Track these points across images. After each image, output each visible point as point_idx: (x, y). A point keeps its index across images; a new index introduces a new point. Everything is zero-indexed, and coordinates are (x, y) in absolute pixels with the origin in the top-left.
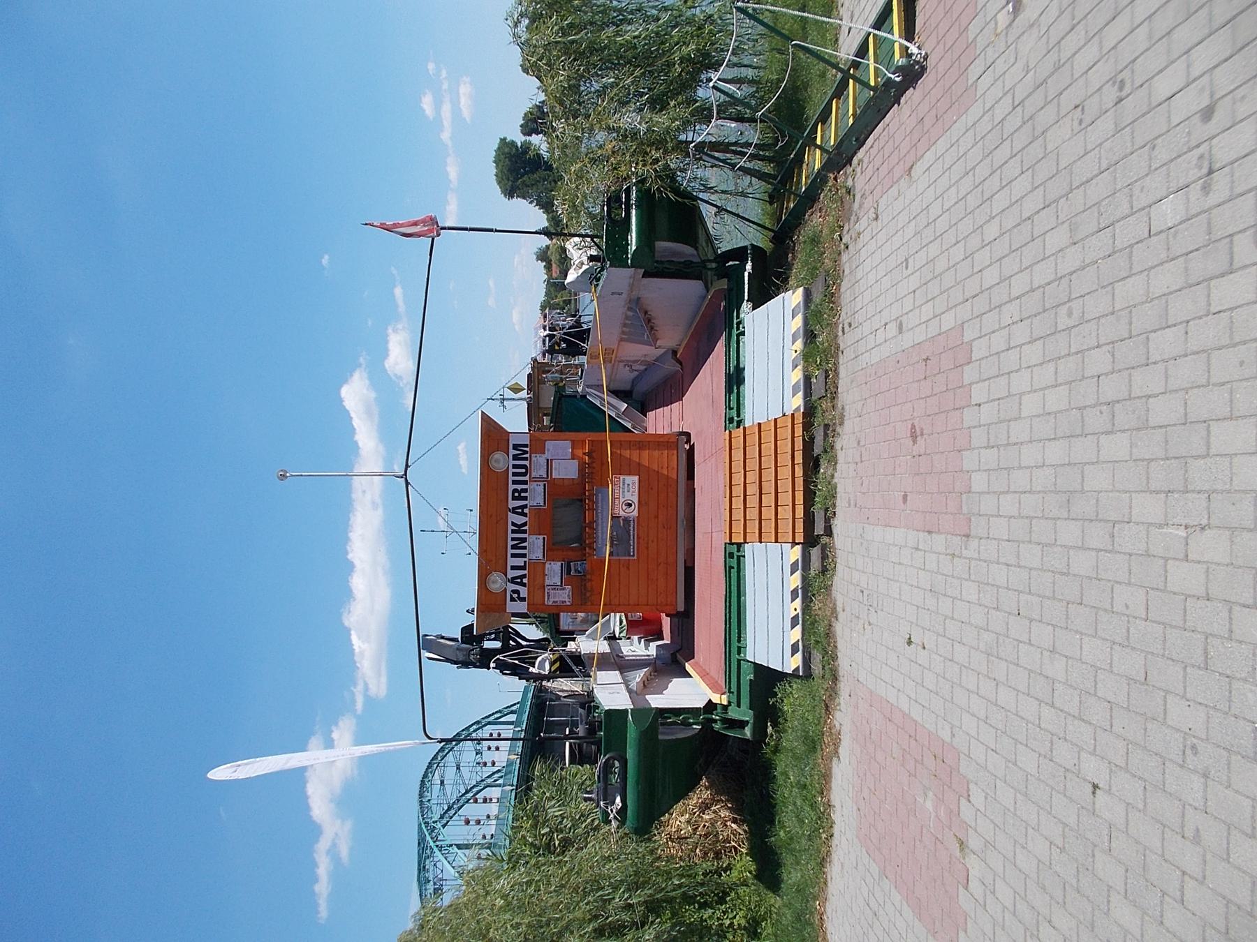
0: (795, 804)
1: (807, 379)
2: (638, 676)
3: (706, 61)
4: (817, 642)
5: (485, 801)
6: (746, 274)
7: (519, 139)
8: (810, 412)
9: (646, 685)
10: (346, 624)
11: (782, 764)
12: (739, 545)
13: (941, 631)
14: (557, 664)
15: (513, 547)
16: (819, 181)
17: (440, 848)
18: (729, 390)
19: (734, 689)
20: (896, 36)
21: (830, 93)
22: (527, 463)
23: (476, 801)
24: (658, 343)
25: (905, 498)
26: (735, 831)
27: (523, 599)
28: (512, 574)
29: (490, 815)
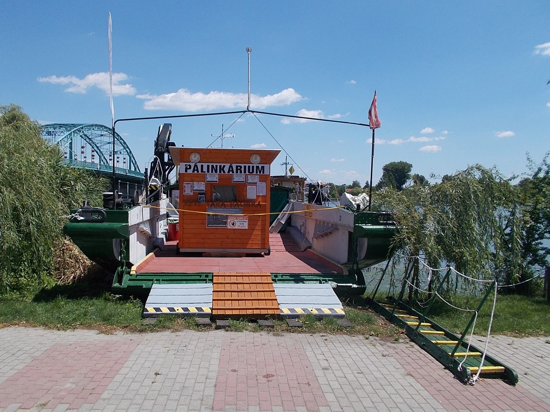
0: (77, 310)
1: (298, 316)
2: (147, 229)
3: (461, 266)
4: (160, 322)
5: (93, 156)
6: (351, 285)
7: (412, 173)
8: (281, 318)
9: (141, 233)
10: (180, 90)
11: (99, 303)
12: (212, 280)
13: (162, 393)
14: (154, 189)
15: (213, 166)
16: (401, 324)
17: (70, 134)
18: (292, 275)
19: (139, 277)
20: (482, 368)
21: (447, 330)
22: (255, 173)
23: (93, 151)
24: (315, 239)
25: (234, 371)
26: (70, 277)
27: (186, 171)
28: (199, 165)
29: (84, 156)
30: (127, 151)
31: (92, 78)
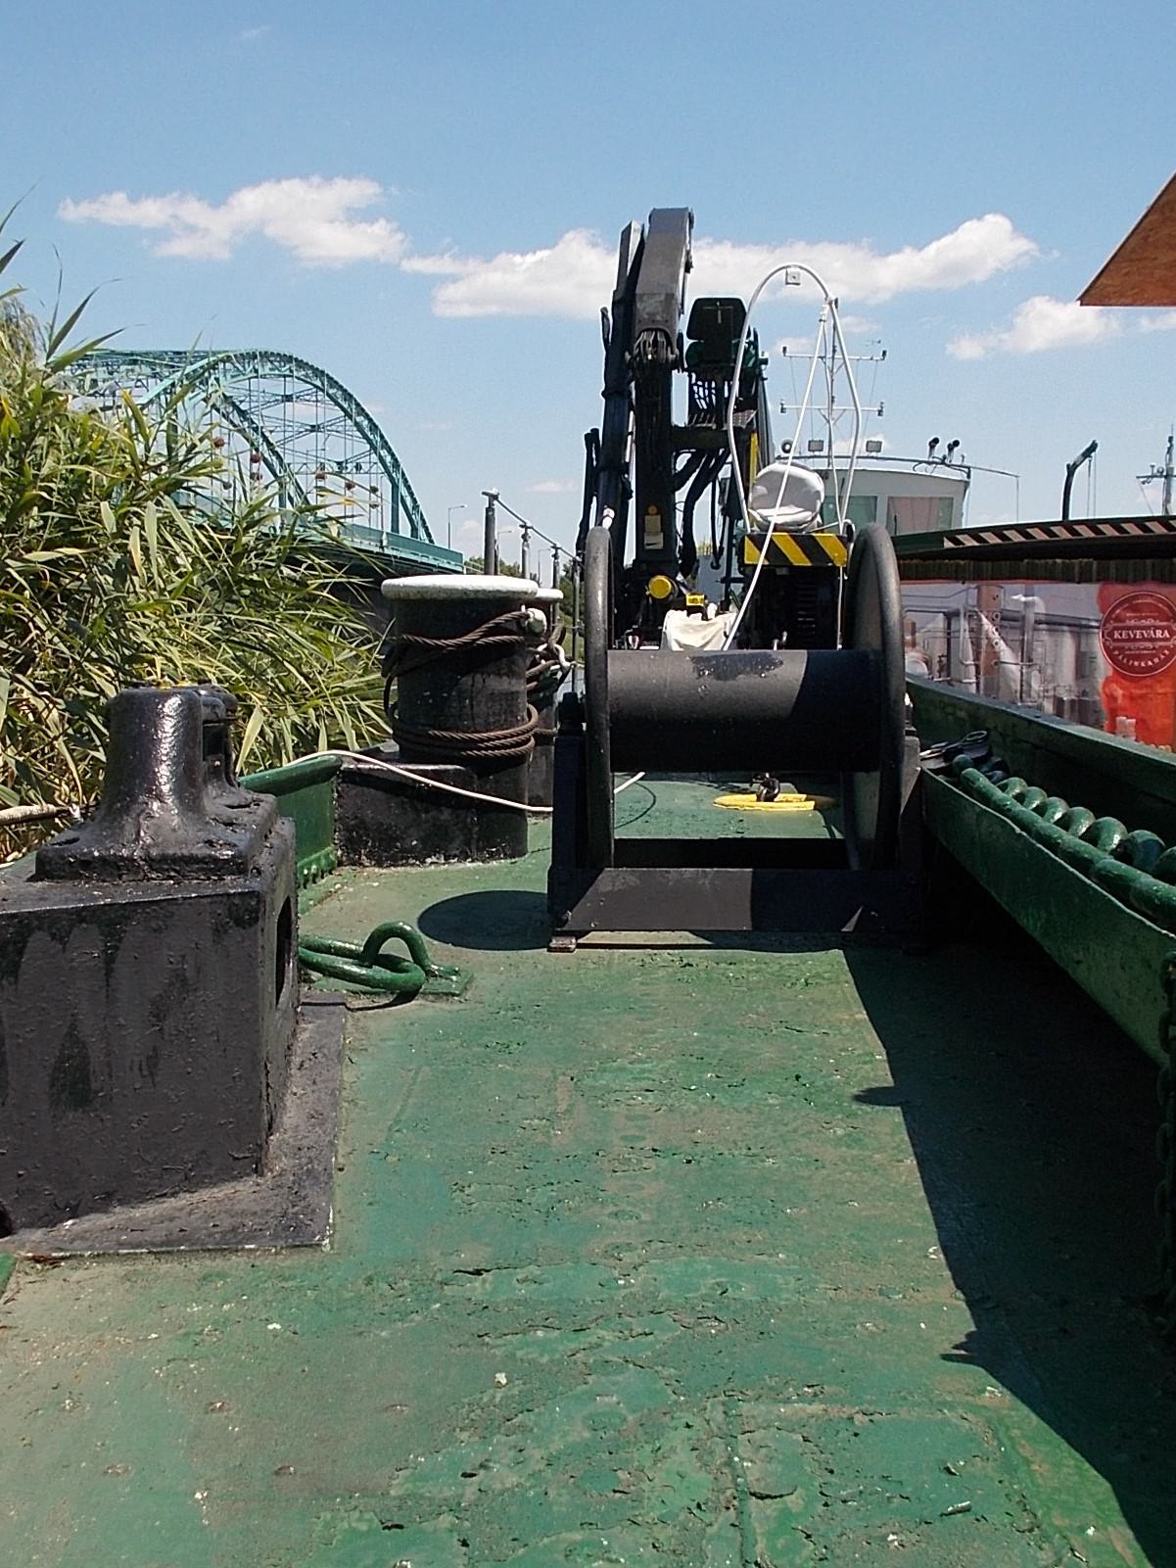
10: (569, 236)
14: (798, 558)
23: (254, 460)
30: (382, 460)
31: (252, 202)
